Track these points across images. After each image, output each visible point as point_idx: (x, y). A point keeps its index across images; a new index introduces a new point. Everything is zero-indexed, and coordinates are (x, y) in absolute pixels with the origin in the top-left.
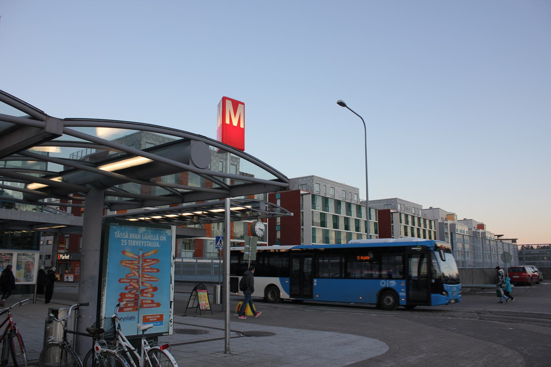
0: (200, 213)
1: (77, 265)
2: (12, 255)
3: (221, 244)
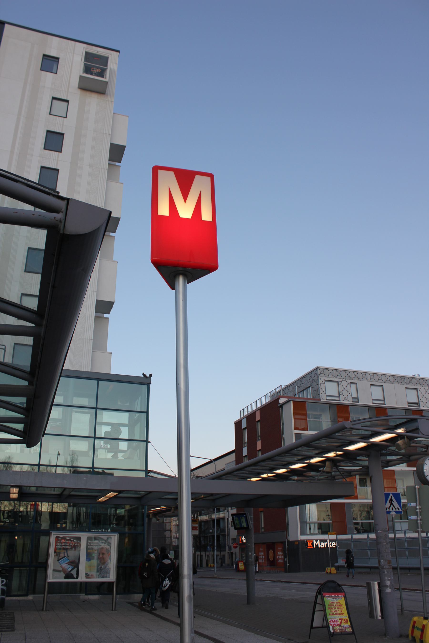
0: (331, 455)
1: (261, 549)
2: (79, 539)
3: (392, 506)
